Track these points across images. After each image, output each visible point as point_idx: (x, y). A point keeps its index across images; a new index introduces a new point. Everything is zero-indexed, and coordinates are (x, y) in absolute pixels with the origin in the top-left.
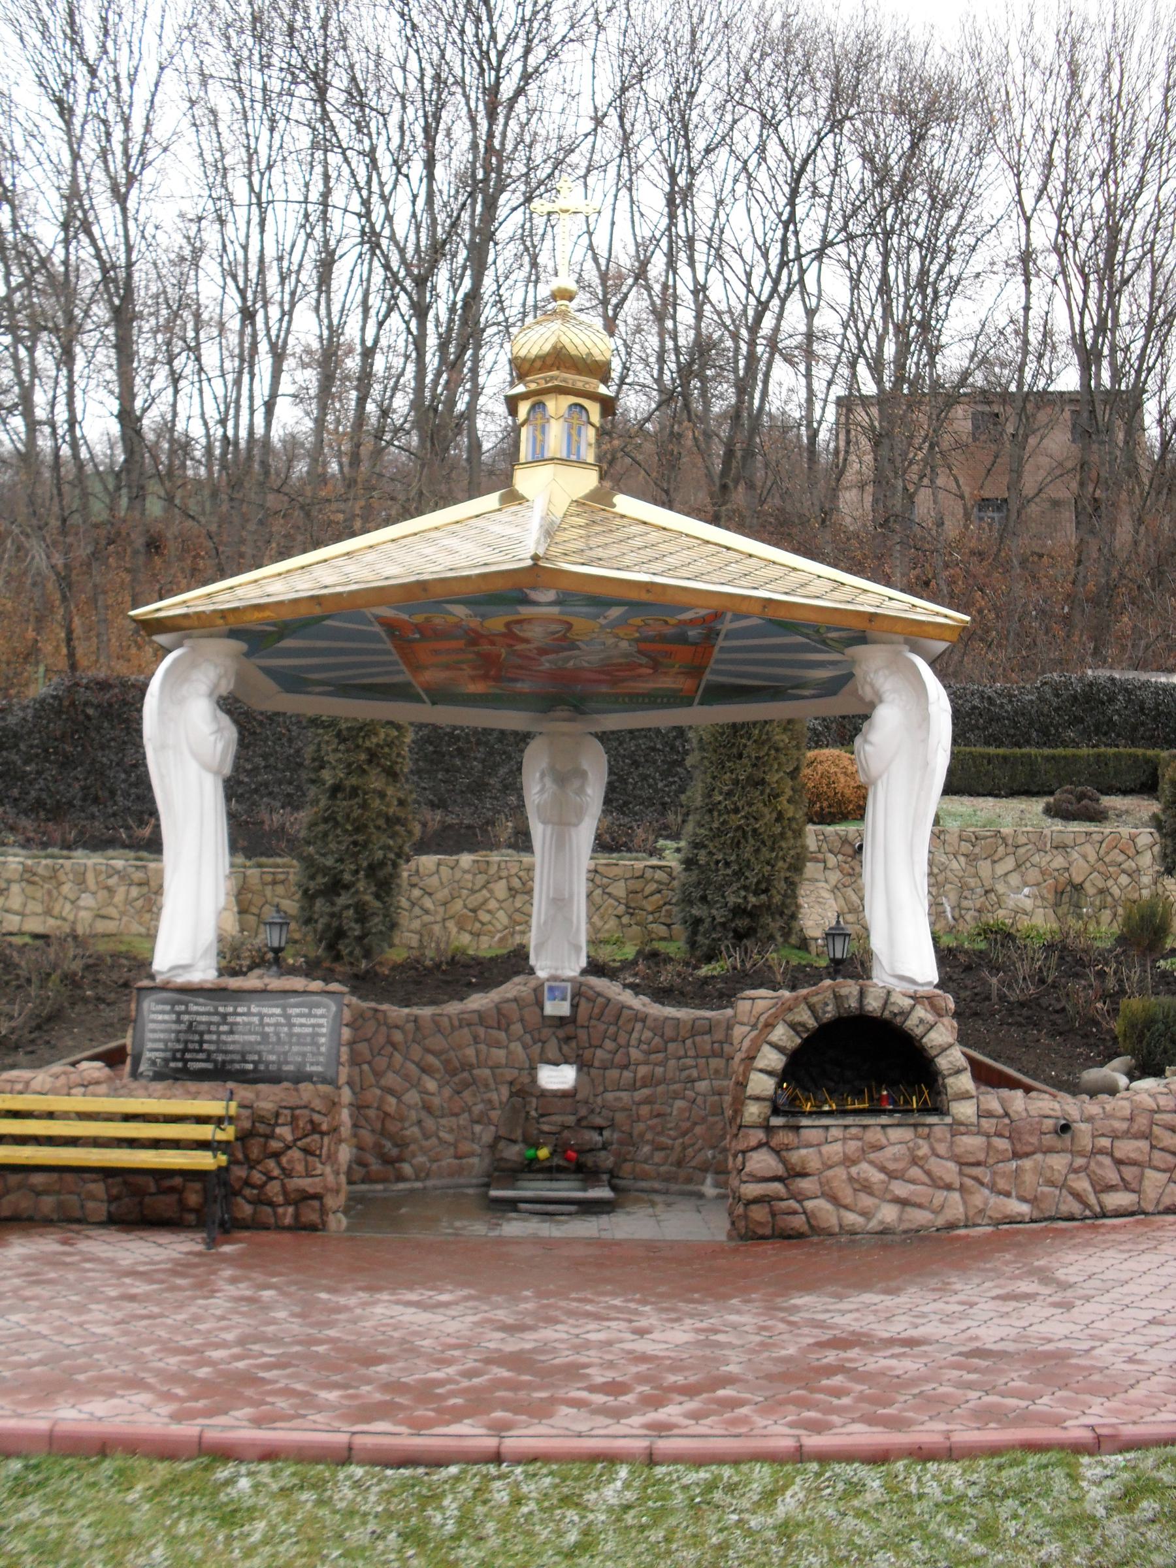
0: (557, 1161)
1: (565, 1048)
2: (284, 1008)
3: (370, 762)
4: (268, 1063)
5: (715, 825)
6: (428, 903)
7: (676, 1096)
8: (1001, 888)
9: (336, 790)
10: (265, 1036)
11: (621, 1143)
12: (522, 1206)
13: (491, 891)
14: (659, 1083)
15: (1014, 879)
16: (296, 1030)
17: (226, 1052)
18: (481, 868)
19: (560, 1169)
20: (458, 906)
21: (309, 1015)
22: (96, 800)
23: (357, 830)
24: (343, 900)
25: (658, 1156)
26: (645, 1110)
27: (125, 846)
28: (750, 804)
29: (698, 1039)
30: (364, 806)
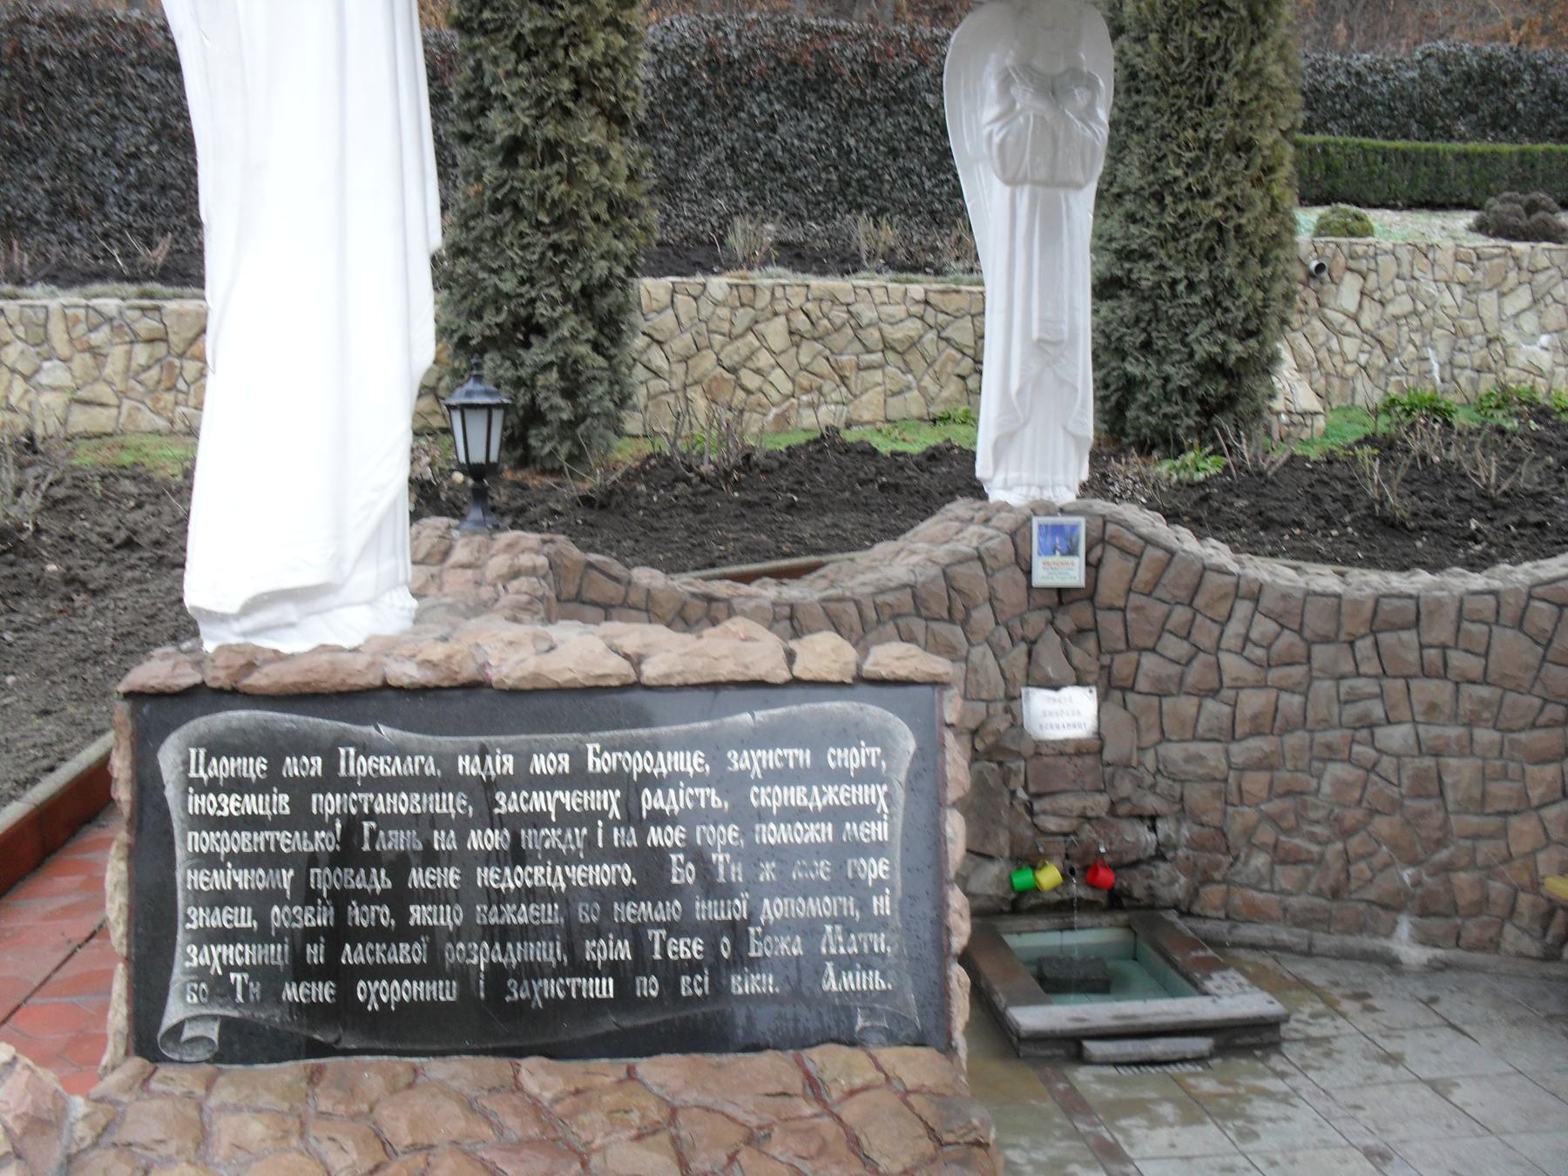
0: (1077, 890)
1: (1076, 652)
2: (715, 749)
3: (576, 95)
4: (671, 971)
5: (1169, 218)
6: (657, 358)
7: (1330, 754)
8: (1509, 335)
9: (513, 149)
10: (651, 863)
11: (1196, 845)
12: (1094, 1048)
13: (761, 337)
14: (1288, 729)
15: (1529, 322)
16: (772, 834)
17: (502, 935)
18: (744, 298)
19: (1086, 906)
20: (707, 362)
21: (820, 774)
22: (74, 213)
23: (559, 223)
24: (537, 353)
25: (1286, 877)
26: (1256, 782)
27: (121, 278)
28: (1230, 184)
29: (1386, 638)
30: (571, 177)
